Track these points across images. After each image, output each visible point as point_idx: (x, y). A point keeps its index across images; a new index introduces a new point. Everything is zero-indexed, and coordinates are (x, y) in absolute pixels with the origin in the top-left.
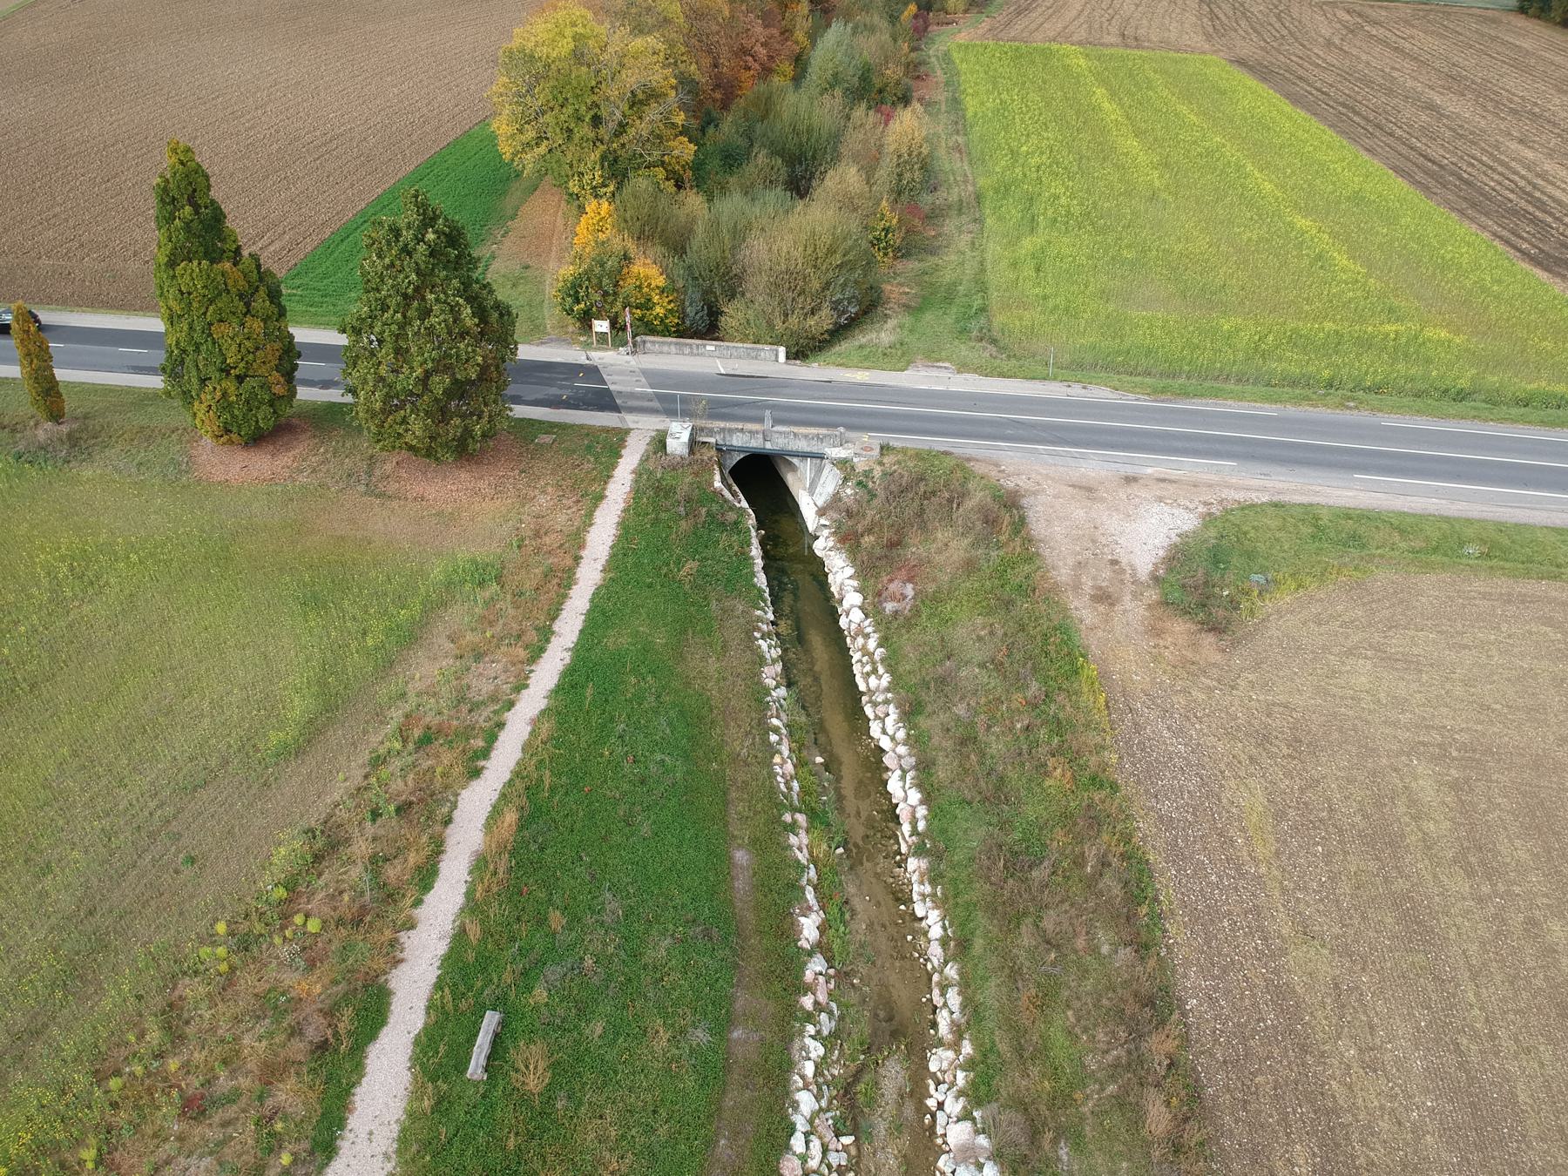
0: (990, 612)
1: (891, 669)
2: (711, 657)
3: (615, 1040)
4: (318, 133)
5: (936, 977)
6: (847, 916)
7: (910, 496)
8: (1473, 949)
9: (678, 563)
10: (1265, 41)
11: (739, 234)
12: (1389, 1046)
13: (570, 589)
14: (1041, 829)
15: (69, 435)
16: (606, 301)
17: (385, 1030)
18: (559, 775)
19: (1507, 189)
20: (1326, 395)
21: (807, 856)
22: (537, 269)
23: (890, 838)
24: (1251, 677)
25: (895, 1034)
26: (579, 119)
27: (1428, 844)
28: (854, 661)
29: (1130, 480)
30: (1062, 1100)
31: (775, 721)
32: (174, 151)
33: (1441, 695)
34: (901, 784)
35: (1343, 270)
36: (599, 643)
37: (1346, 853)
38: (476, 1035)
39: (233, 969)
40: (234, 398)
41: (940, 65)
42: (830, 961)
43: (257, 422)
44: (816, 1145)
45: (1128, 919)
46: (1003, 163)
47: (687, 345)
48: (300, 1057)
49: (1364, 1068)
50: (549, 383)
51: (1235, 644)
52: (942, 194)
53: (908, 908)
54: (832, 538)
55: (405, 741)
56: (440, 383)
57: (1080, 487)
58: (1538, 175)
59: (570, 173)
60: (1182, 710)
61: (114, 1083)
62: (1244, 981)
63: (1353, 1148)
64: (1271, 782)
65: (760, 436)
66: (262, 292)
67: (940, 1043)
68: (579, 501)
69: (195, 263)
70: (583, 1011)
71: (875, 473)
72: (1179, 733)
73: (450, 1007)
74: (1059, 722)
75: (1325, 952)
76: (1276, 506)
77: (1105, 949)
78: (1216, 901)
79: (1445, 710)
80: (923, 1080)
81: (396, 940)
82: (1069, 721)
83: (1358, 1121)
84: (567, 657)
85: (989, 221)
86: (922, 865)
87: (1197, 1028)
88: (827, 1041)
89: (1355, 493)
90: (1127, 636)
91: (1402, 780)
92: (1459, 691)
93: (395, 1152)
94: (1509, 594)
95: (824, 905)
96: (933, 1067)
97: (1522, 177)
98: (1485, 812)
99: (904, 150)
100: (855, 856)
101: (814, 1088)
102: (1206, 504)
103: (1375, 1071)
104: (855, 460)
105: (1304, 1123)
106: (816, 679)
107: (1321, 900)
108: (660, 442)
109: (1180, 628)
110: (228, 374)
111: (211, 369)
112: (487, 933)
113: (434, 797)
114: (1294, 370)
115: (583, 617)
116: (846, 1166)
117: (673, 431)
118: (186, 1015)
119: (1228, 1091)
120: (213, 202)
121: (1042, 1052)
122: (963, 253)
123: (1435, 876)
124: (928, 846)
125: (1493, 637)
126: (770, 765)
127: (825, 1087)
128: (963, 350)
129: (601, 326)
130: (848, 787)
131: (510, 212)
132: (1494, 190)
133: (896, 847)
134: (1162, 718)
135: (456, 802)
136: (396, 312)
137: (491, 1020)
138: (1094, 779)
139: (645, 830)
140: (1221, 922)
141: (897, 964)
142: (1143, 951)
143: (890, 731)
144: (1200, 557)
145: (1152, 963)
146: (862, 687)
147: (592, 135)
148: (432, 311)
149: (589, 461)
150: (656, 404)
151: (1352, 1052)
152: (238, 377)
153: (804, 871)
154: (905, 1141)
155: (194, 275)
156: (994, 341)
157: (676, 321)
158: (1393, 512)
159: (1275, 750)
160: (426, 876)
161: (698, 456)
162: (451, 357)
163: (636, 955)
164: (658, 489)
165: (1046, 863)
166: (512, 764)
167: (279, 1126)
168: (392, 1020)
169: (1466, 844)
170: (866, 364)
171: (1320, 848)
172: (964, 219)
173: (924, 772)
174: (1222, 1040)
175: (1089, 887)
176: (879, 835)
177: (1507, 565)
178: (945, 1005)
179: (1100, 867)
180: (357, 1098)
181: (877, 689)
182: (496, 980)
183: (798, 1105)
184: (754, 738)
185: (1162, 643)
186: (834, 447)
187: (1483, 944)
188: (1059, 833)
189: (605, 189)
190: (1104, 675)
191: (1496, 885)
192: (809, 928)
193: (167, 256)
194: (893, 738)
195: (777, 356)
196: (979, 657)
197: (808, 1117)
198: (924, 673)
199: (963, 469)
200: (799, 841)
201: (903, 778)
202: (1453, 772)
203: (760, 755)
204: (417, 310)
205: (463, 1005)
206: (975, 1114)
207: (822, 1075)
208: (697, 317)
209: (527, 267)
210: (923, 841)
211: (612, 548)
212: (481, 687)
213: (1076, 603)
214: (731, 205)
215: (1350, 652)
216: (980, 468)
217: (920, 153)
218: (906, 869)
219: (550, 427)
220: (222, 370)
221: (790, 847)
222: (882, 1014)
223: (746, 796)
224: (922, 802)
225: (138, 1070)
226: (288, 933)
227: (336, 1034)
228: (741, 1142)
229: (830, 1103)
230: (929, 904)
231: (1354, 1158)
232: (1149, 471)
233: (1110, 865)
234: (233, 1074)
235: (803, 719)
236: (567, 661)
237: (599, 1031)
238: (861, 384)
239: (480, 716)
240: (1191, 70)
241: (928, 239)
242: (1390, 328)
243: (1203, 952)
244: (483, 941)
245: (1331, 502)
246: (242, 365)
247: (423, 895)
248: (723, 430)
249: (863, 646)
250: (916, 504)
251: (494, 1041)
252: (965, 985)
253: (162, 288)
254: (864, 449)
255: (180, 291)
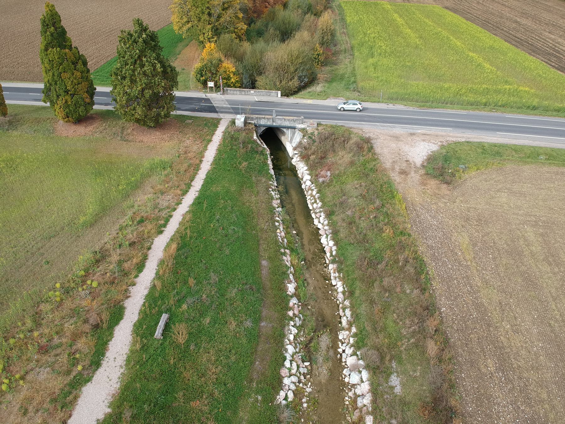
0: (360, 178)
1: (322, 201)
2: (252, 196)
3: (214, 325)
4: (107, 28)
5: (341, 306)
6: (306, 285)
7: (329, 140)
8: (553, 290)
9: (240, 163)
10: (455, 2)
11: (262, 53)
12: (523, 324)
13: (198, 171)
14: (381, 251)
15: (9, 121)
16: (212, 77)
17: (122, 321)
18: (194, 233)
19: (545, 47)
20: (484, 108)
21: (290, 263)
22: (187, 70)
23: (322, 258)
24: (461, 199)
25: (325, 326)
26: (203, 13)
27: (532, 254)
28: (307, 199)
29: (412, 134)
30: (393, 346)
31: (277, 218)
32: (48, 6)
33: (534, 204)
34: (326, 239)
35: (488, 69)
36: (209, 189)
37: (501, 258)
38: (158, 323)
39: (62, 300)
40: (70, 103)
41: (337, 8)
42: (299, 300)
43: (79, 113)
44: (294, 365)
45: (417, 280)
46: (361, 36)
47: (243, 91)
48: (88, 331)
49: (513, 332)
50: (191, 104)
51: (454, 188)
52: (338, 46)
53: (329, 282)
54: (299, 157)
55: (133, 222)
56: (148, 93)
57: (394, 137)
58: (556, 43)
59: (200, 34)
60: (435, 210)
61: (12, 341)
62: (464, 302)
63: (512, 361)
64: (470, 234)
65: (271, 120)
66: (80, 62)
67: (343, 329)
68: (202, 142)
69: (55, 49)
70: (202, 314)
71: (315, 133)
72: (434, 217)
73: (148, 312)
74: (387, 214)
75: (495, 291)
76: (468, 142)
77: (408, 291)
78: (451, 274)
79: (536, 210)
80: (337, 342)
81: (128, 289)
82: (391, 213)
83: (512, 351)
84: (197, 194)
85: (356, 54)
86: (334, 266)
87: (446, 318)
88: (299, 328)
89: (498, 138)
90: (413, 186)
91: (521, 233)
92: (541, 203)
93: (125, 365)
94: (557, 172)
95: (297, 281)
96: (340, 337)
97: (551, 43)
98: (554, 244)
99: (324, 27)
100: (309, 264)
101: (293, 344)
102: (441, 142)
103: (518, 333)
104: (308, 128)
105: (491, 352)
106: (293, 205)
107: (492, 273)
108: (233, 122)
109: (433, 183)
110: (68, 93)
111: (61, 91)
112: (163, 286)
113: (144, 241)
114: (472, 99)
115: (203, 180)
116: (307, 373)
117: (238, 118)
118: (42, 317)
119: (460, 340)
120: (62, 26)
121: (384, 329)
122: (347, 65)
123: (536, 265)
124: (337, 260)
125: (552, 186)
126: (276, 233)
127: (298, 344)
128: (348, 94)
129: (211, 84)
130: (306, 241)
131: (178, 52)
132: (541, 47)
133: (324, 261)
134: (427, 213)
135: (153, 242)
136: (131, 65)
137: (164, 317)
138: (401, 233)
139: (227, 252)
140: (454, 281)
141: (325, 301)
142: (423, 291)
143: (322, 222)
144: (440, 159)
145: (427, 294)
146: (311, 208)
147: (208, 19)
148: (145, 65)
149: (206, 129)
150: (231, 111)
151: (508, 326)
152: (71, 95)
153: (289, 269)
154: (330, 364)
155: (54, 53)
156: (359, 92)
157: (239, 85)
158: (512, 144)
159: (472, 223)
160: (140, 267)
161: (247, 127)
162: (152, 83)
163: (223, 295)
164: (232, 138)
165: (383, 262)
166: (175, 229)
167: (78, 356)
168: (125, 317)
169: (547, 254)
170: (311, 98)
171: (491, 256)
172: (347, 54)
173: (335, 235)
174: (456, 322)
175: (401, 270)
176: (318, 257)
177: (556, 162)
178: (345, 315)
179: (405, 263)
180: (110, 346)
181: (317, 208)
182: (167, 303)
183: (287, 350)
184: (269, 223)
185: (426, 188)
186: (299, 124)
187: (557, 289)
188: (388, 252)
189: (213, 39)
190: (405, 199)
191: (560, 268)
192: (291, 288)
193: (44, 46)
194: (323, 224)
195: (277, 95)
196: (356, 194)
197: (291, 355)
198: (334, 201)
199: (349, 131)
200: (287, 260)
201: (327, 237)
202: (541, 230)
203: (272, 229)
204: (139, 64)
205: (154, 311)
206: (358, 353)
207: (297, 340)
208: (247, 84)
209: (184, 69)
210: (335, 258)
211: (214, 157)
212: (164, 202)
213: (393, 175)
214: (260, 44)
215: (498, 191)
216: (355, 131)
217: (330, 29)
218: (328, 269)
219: (191, 118)
220: (65, 92)
221: (284, 260)
222: (320, 319)
223: (266, 243)
224: (334, 245)
225: (22, 336)
226: (84, 287)
227: (101, 321)
228: (265, 363)
229: (300, 350)
230: (337, 280)
231: (512, 365)
232: (419, 131)
233: (409, 262)
234: (60, 337)
235: (288, 218)
236: (197, 195)
237: (208, 321)
238: (308, 104)
239: (163, 213)
240: (429, 9)
241: (334, 60)
242: (507, 87)
243: (447, 292)
244: (162, 289)
245: (488, 141)
246: (73, 90)
247: (139, 273)
248: (257, 118)
249: (311, 194)
250: (331, 143)
251: (166, 325)
252: (352, 307)
253: (42, 60)
254: (311, 124)
255: (49, 60)
